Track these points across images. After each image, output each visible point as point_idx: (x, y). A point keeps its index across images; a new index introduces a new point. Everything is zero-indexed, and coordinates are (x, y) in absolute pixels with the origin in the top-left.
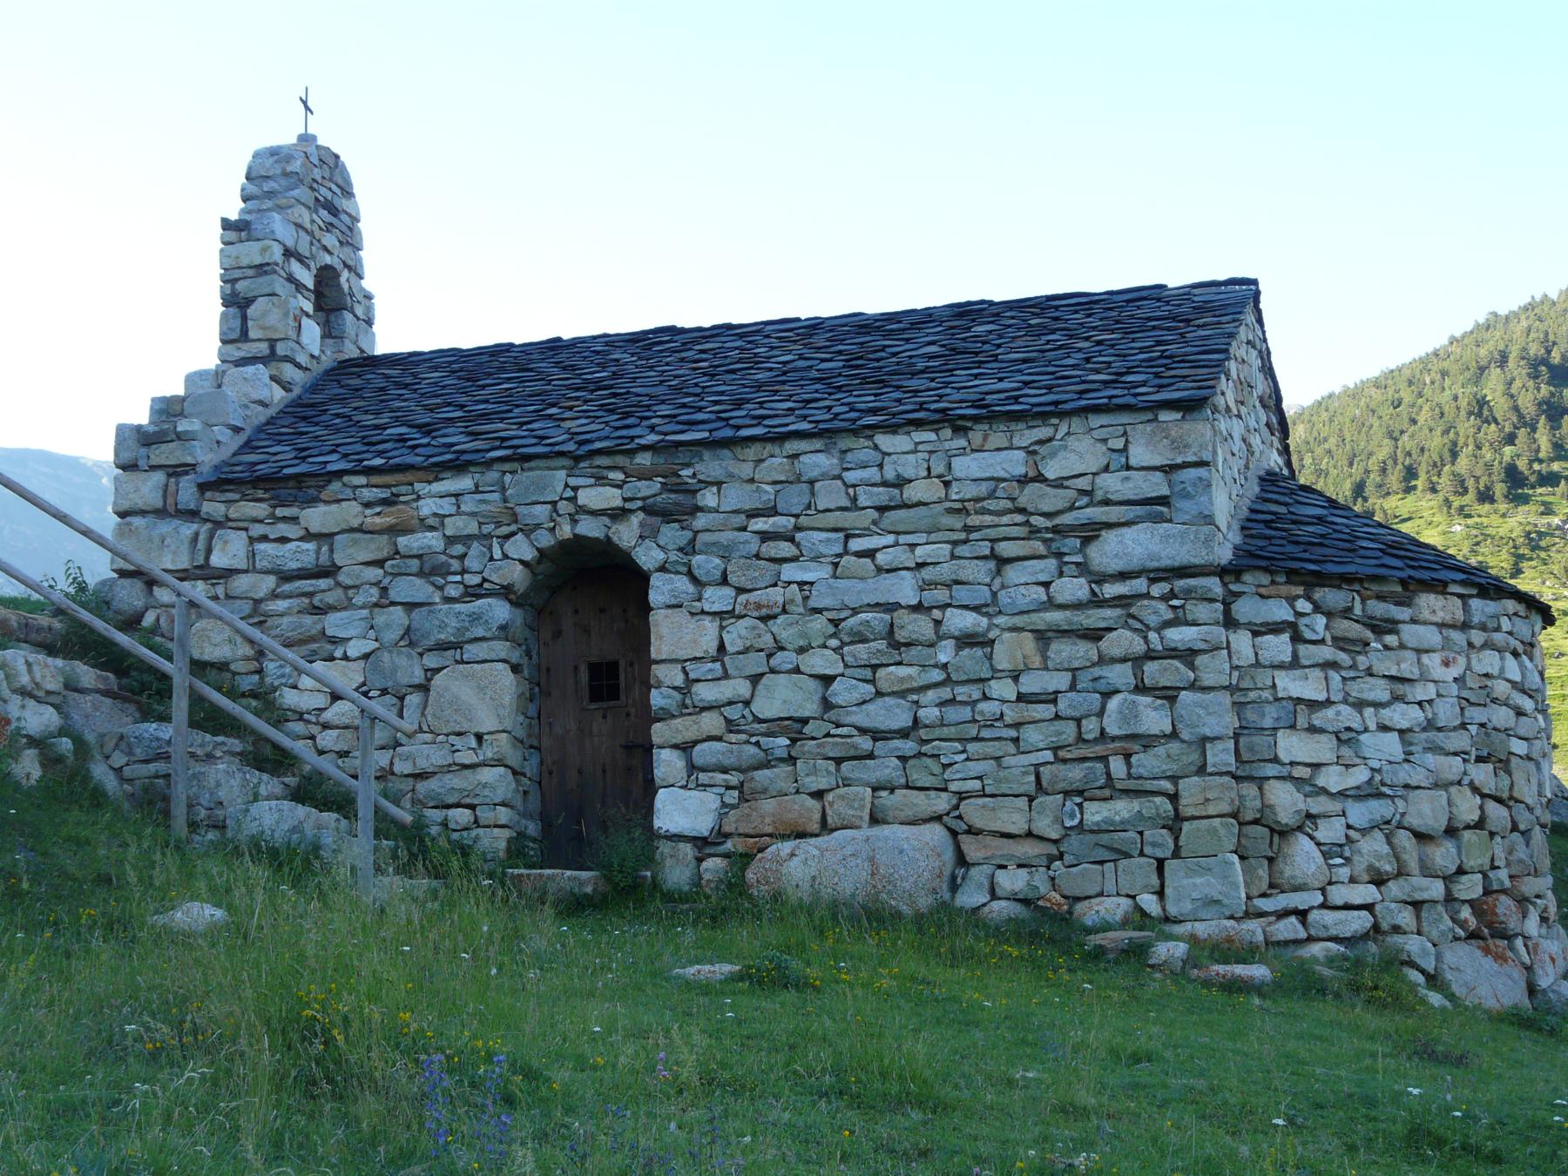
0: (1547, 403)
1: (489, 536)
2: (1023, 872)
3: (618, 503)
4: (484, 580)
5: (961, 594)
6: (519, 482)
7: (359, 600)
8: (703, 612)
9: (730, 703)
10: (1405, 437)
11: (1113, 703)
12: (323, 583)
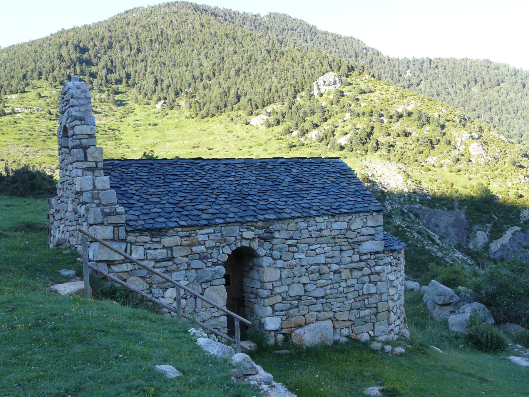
0: (79, 58)
1: (219, 247)
2: (347, 329)
3: (253, 236)
4: (218, 260)
5: (335, 260)
6: (226, 230)
7: (181, 268)
8: (276, 268)
9: (283, 292)
10: (39, 63)
11: (365, 286)
12: (171, 263)
